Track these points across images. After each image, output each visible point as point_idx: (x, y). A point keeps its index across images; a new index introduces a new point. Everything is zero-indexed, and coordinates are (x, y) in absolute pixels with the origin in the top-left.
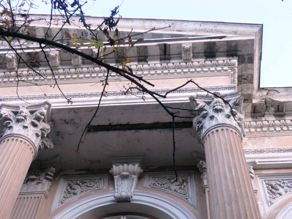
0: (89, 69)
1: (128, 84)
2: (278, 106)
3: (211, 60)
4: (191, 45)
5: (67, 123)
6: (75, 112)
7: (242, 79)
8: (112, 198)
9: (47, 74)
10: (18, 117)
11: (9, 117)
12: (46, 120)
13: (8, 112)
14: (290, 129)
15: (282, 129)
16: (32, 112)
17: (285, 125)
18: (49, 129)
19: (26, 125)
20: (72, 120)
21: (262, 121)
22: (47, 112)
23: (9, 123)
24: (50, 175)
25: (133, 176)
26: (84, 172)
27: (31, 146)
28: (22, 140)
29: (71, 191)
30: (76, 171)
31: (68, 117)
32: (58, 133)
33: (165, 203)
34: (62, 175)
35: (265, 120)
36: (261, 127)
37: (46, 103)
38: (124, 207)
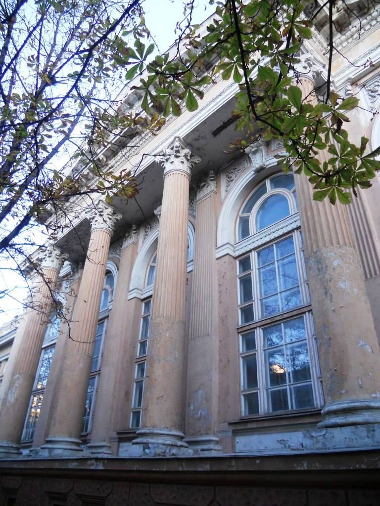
1: (104, 221)
2: (358, 6)
5: (198, 140)
6: (197, 131)
7: (309, 9)
8: (253, 172)
11: (162, 160)
12: (184, 147)
14: (378, 20)
15: (371, 26)
16: (172, 149)
17: (373, 20)
19: (171, 161)
20: (199, 136)
21: (350, 30)
23: (163, 165)
25: (260, 148)
26: (233, 161)
27: (181, 173)
28: (173, 172)
29: (230, 180)
30: (228, 163)
31: (196, 135)
32: (198, 149)
34: (221, 171)
35: (353, 27)
36: (352, 36)
37: (175, 138)
38: (263, 174)
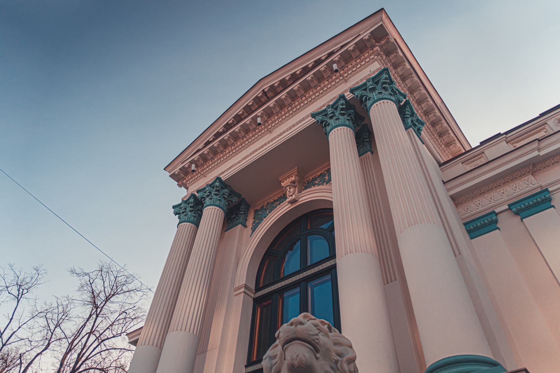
0: (353, 65)
3: (367, 52)
4: (312, 76)
9: (318, 91)
10: (329, 116)
13: (321, 118)
18: (227, 192)
22: (345, 102)
24: (408, 115)
33: (319, 193)
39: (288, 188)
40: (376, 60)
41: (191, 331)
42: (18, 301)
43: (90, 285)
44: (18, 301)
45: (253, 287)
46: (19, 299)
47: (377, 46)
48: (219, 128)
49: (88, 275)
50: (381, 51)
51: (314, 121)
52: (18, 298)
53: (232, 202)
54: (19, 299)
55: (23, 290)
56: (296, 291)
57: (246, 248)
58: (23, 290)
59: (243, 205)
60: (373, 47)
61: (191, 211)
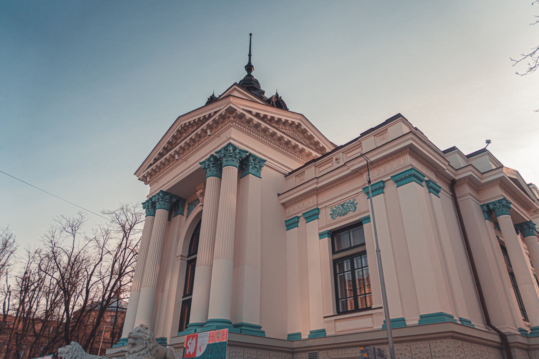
39: (199, 197)
40: (232, 126)
41: (152, 286)
42: (74, 236)
43: (117, 221)
44: (74, 236)
45: (186, 254)
46: (74, 234)
47: (231, 117)
48: (165, 144)
49: (114, 213)
50: (234, 119)
51: (200, 167)
52: (73, 234)
53: (172, 202)
54: (74, 234)
55: (75, 227)
56: (331, 147)
57: (184, 226)
58: (75, 227)
59: (180, 201)
60: (229, 118)
61: (151, 208)
